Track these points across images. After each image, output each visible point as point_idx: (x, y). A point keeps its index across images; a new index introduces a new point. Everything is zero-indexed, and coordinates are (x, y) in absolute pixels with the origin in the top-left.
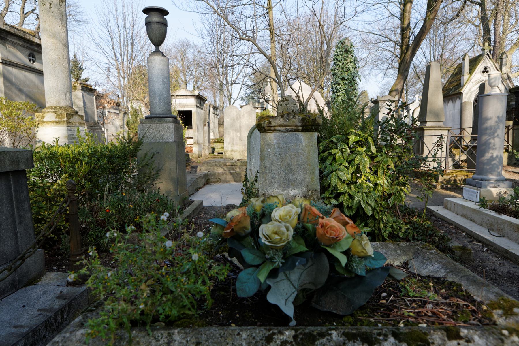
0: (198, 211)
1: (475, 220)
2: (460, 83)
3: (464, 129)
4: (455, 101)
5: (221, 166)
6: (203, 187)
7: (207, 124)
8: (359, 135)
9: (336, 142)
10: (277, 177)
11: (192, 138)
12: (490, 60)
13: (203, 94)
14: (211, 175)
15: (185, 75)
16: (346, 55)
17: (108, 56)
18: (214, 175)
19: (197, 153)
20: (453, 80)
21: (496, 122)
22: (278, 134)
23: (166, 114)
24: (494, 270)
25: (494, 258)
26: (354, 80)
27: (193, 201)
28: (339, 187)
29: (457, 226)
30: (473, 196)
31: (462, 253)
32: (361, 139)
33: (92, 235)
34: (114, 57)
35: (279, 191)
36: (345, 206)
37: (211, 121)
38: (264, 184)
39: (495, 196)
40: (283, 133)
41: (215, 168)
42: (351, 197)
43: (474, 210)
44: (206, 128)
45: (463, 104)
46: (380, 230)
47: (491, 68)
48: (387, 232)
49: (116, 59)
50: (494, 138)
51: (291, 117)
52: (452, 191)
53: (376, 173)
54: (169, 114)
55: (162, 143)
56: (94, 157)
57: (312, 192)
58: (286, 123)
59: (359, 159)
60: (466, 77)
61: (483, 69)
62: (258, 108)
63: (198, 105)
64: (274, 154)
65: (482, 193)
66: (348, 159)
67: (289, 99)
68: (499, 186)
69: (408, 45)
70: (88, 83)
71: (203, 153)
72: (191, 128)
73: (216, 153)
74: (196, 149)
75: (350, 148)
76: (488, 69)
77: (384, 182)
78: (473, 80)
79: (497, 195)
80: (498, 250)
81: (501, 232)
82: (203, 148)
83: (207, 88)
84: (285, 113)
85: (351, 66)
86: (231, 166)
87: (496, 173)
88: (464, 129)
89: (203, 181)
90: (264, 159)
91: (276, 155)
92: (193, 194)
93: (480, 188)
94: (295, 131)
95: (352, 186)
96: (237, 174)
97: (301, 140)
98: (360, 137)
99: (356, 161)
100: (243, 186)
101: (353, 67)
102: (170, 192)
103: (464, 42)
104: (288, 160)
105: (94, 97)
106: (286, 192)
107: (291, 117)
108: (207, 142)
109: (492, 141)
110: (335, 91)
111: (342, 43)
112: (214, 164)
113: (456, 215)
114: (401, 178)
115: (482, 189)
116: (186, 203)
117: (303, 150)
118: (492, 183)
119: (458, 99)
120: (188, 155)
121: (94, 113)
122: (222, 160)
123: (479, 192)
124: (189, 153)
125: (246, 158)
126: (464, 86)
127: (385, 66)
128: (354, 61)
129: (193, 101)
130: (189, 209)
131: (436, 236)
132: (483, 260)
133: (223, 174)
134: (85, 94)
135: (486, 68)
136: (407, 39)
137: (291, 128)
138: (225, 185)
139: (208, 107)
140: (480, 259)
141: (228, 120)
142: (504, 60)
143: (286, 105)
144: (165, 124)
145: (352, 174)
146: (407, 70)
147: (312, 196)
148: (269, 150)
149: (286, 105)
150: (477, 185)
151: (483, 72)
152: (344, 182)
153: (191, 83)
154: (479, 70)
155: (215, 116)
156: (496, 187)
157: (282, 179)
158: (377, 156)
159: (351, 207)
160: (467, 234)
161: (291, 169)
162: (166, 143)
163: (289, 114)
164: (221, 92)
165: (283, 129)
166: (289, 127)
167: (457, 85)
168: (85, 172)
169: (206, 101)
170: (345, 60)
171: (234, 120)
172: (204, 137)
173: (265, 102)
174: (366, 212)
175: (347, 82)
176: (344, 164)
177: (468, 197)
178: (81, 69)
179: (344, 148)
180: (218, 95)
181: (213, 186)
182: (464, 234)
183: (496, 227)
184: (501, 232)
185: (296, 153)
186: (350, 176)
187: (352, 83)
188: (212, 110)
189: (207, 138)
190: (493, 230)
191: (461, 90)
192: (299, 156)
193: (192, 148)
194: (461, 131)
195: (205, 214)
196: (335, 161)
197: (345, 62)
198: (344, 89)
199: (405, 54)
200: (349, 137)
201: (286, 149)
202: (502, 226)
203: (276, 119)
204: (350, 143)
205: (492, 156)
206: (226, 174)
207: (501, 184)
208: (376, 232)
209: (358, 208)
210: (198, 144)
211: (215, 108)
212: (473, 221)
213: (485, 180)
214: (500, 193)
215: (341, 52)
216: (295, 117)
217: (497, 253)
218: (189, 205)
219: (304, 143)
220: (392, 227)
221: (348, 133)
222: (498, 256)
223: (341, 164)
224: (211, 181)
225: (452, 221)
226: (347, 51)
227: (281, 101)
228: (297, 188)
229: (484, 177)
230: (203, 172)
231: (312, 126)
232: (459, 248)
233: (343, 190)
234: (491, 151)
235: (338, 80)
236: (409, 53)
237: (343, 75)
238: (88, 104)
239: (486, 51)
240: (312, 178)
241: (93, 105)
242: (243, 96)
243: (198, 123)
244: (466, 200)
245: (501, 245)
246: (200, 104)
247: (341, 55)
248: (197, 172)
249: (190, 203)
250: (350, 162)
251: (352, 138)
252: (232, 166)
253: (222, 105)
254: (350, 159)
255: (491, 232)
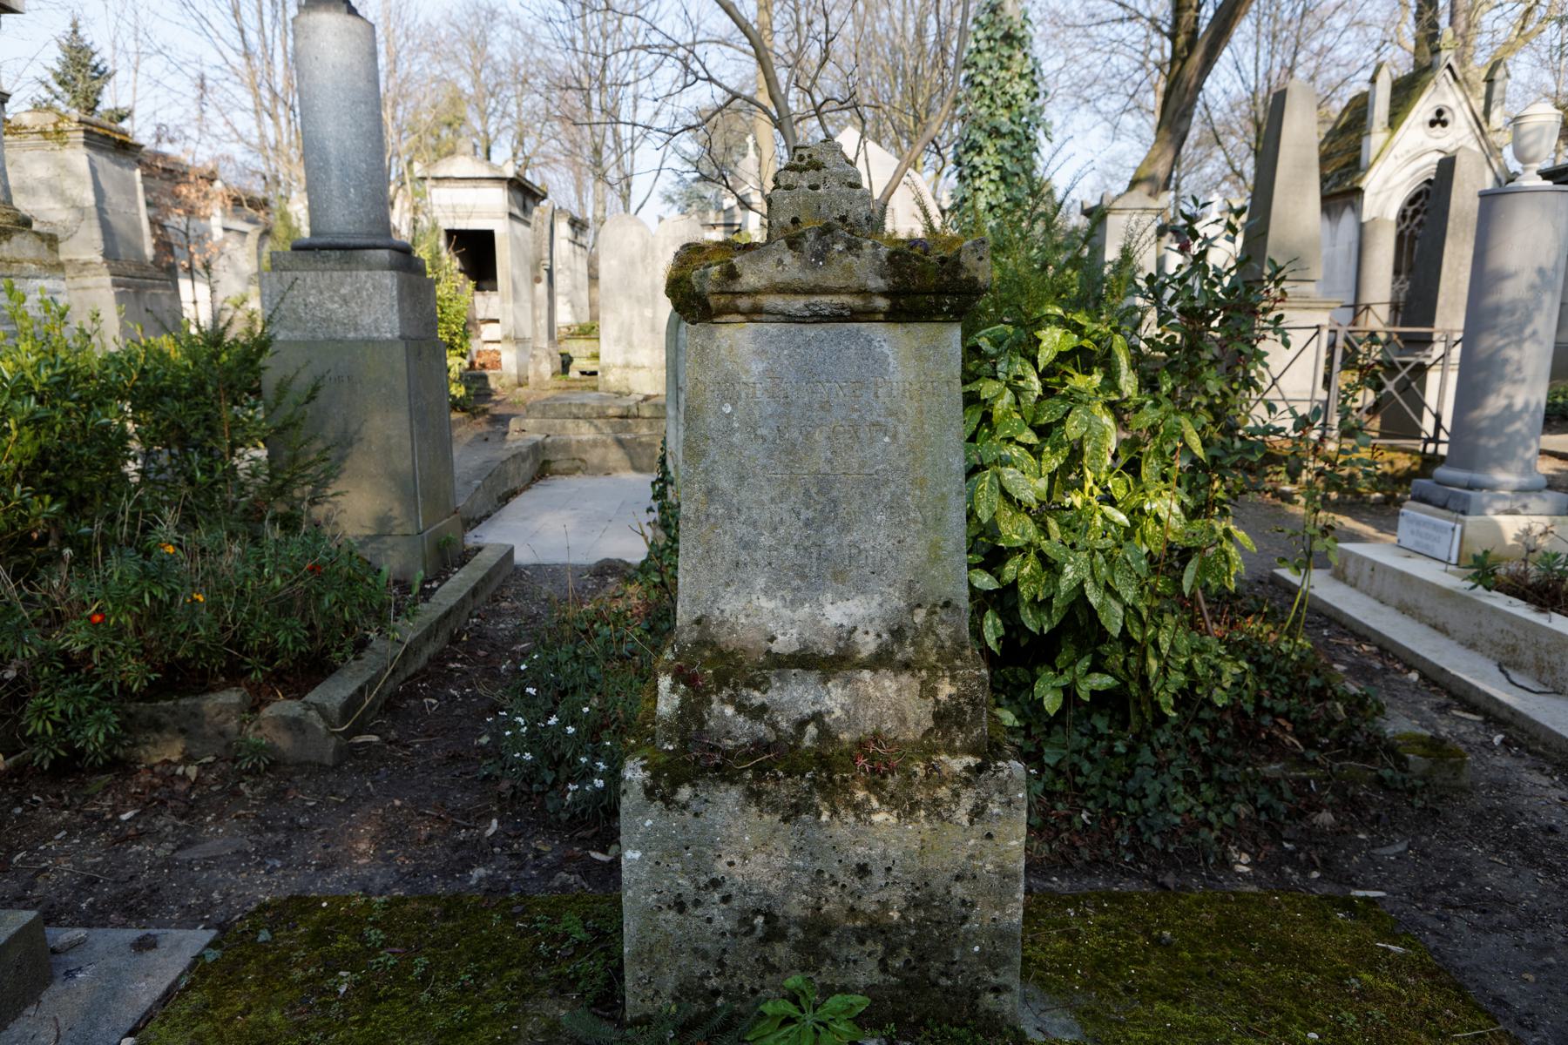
0: (494, 586)
1: (1450, 627)
2: (1357, 160)
3: (1368, 307)
4: (1339, 215)
5: (587, 418)
6: (527, 487)
7: (544, 275)
8: (1078, 329)
9: (993, 351)
10: (766, 540)
11: (497, 321)
12: (1455, 86)
13: (542, 178)
14: (555, 447)
15: (484, 115)
16: (1006, 51)
17: (220, 43)
18: (566, 447)
19: (514, 371)
20: (1333, 148)
21: (1532, 287)
22: (773, 329)
23: (369, 235)
24: (1552, 830)
25: (1536, 778)
26: (1028, 139)
27: (479, 549)
28: (1002, 526)
29: (1387, 645)
30: (1437, 540)
31: (1434, 763)
32: (1086, 343)
33: (42, 708)
34: (239, 46)
35: (772, 605)
36: (1026, 597)
37: (558, 266)
38: (704, 575)
39: (1510, 541)
40: (794, 327)
41: (570, 423)
42: (1050, 567)
43: (1447, 594)
44: (542, 288)
45: (1368, 228)
46: (1144, 681)
47: (1458, 113)
48: (1172, 690)
49: (247, 55)
50: (1519, 343)
51: (839, 247)
52: (1345, 514)
53: (1133, 467)
54: (378, 235)
55: (354, 342)
56: (67, 398)
57: (931, 613)
58: (810, 278)
59: (1082, 422)
60: (1377, 138)
61: (1432, 115)
62: (714, 226)
63: (517, 211)
64: (751, 428)
65: (1469, 531)
66: (1035, 417)
67: (829, 160)
68: (1525, 507)
69: (1195, 32)
70: (125, 125)
71: (531, 373)
72: (494, 289)
73: (574, 373)
74: (509, 359)
75: (1041, 376)
76: (1446, 116)
77: (1166, 505)
78: (1399, 150)
79: (1517, 538)
80: (1545, 745)
81: (1547, 677)
82: (533, 356)
83: (556, 161)
84: (809, 225)
85: (1020, 88)
86: (621, 417)
87: (1517, 465)
88: (1368, 307)
89: (527, 468)
90: (704, 454)
91: (763, 431)
92: (488, 516)
93: (1464, 513)
94: (856, 316)
95: (1053, 524)
96: (640, 444)
97: (882, 361)
98: (1081, 336)
99: (1073, 430)
100: (654, 498)
101: (1027, 94)
102: (390, 519)
103: (1351, 34)
104: (819, 460)
105: (138, 173)
106: (807, 608)
107: (839, 247)
108: (545, 336)
109: (1512, 353)
110: (966, 172)
111: (993, 11)
112: (565, 410)
113: (1376, 604)
114: (1217, 484)
115: (1469, 519)
116: (448, 557)
117: (891, 413)
118: (1504, 498)
119: (1348, 212)
120: (485, 378)
121: (137, 229)
122: (591, 399)
123: (1458, 527)
124: (489, 372)
125: (336, 705)
126: (1369, 167)
127: (1115, 103)
128: (1033, 72)
129: (498, 197)
130: (460, 582)
131: (1338, 699)
132: (1502, 786)
133: (595, 444)
134: (102, 160)
135: (1440, 112)
136: (1192, 12)
137: (836, 300)
138: (601, 482)
139: (548, 219)
140: (1492, 784)
141: (614, 262)
142: (1498, 86)
143: (814, 187)
144: (363, 274)
145: (1052, 476)
146: (1186, 115)
147: (930, 629)
148: (728, 409)
149: (814, 187)
150: (1451, 504)
151: (1432, 124)
152: (1018, 506)
153: (503, 141)
154: (1420, 119)
155: (578, 250)
156: (1514, 512)
157: (790, 551)
158: (1138, 408)
159: (1047, 603)
160: (1423, 676)
161: (834, 501)
162: (369, 342)
163: (827, 230)
164: (599, 171)
165: (798, 304)
166: (826, 299)
167: (1346, 165)
168: (25, 457)
169: (544, 197)
170: (1001, 68)
171: (632, 263)
172: (534, 320)
173: (737, 210)
174: (1103, 621)
175: (1007, 143)
176: (1021, 439)
177: (1417, 543)
178: (103, 75)
179: (1022, 378)
180: (589, 181)
181: (559, 486)
182: (1414, 676)
183: (1528, 657)
184: (1547, 677)
185: (855, 427)
186: (1042, 484)
187: (1021, 145)
188: (563, 229)
189: (544, 322)
190: (1518, 666)
191: (1360, 180)
192: (872, 440)
193: (498, 353)
194: (1356, 315)
195: (517, 596)
196: (990, 426)
197: (1003, 74)
198: (997, 168)
199: (1184, 61)
200: (1039, 334)
201: (809, 406)
202: (1555, 658)
203: (761, 257)
204: (1045, 356)
205: (1509, 407)
206: (604, 444)
207: (1534, 503)
208: (1134, 689)
209: (1071, 607)
210: (518, 341)
211: (578, 225)
212: (1440, 628)
213: (1481, 488)
214: (1527, 532)
215: (989, 39)
216: (859, 246)
217: (1542, 755)
218: (463, 564)
219: (898, 377)
220: (1189, 669)
221: (1038, 320)
222: (1548, 768)
223: (1010, 440)
224: (554, 466)
225: (1368, 628)
226: (1009, 38)
227: (789, 168)
228: (861, 589)
229: (1477, 477)
230: (527, 436)
231: (941, 292)
232: (1420, 740)
233: (1017, 540)
234: (1507, 389)
235: (979, 137)
236: (1197, 58)
237: (996, 121)
238: (114, 197)
239: (1444, 54)
240: (935, 546)
241: (134, 203)
242: (671, 188)
243: (517, 272)
244: (1412, 553)
245: (1556, 729)
246: (524, 208)
247: (990, 50)
248: (509, 437)
249: (465, 557)
250: (1043, 432)
251: (1053, 340)
252: (627, 417)
253: (599, 214)
254: (1044, 420)
255: (1510, 671)
